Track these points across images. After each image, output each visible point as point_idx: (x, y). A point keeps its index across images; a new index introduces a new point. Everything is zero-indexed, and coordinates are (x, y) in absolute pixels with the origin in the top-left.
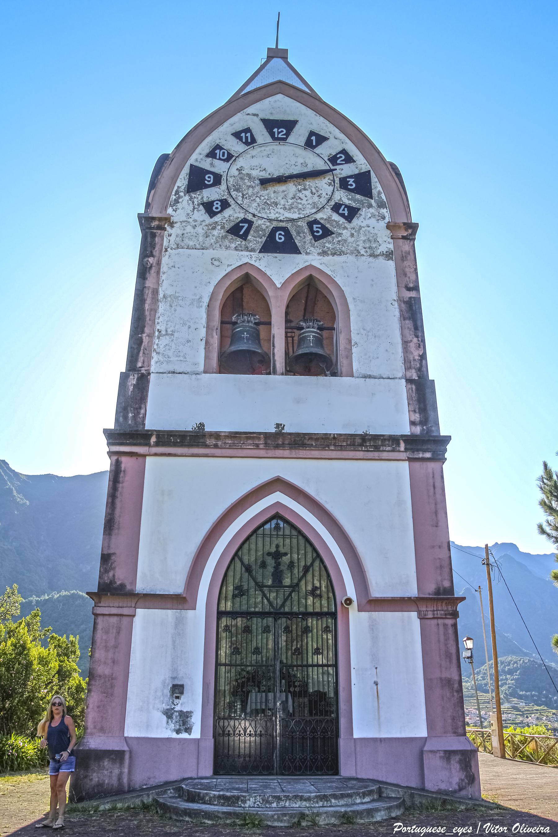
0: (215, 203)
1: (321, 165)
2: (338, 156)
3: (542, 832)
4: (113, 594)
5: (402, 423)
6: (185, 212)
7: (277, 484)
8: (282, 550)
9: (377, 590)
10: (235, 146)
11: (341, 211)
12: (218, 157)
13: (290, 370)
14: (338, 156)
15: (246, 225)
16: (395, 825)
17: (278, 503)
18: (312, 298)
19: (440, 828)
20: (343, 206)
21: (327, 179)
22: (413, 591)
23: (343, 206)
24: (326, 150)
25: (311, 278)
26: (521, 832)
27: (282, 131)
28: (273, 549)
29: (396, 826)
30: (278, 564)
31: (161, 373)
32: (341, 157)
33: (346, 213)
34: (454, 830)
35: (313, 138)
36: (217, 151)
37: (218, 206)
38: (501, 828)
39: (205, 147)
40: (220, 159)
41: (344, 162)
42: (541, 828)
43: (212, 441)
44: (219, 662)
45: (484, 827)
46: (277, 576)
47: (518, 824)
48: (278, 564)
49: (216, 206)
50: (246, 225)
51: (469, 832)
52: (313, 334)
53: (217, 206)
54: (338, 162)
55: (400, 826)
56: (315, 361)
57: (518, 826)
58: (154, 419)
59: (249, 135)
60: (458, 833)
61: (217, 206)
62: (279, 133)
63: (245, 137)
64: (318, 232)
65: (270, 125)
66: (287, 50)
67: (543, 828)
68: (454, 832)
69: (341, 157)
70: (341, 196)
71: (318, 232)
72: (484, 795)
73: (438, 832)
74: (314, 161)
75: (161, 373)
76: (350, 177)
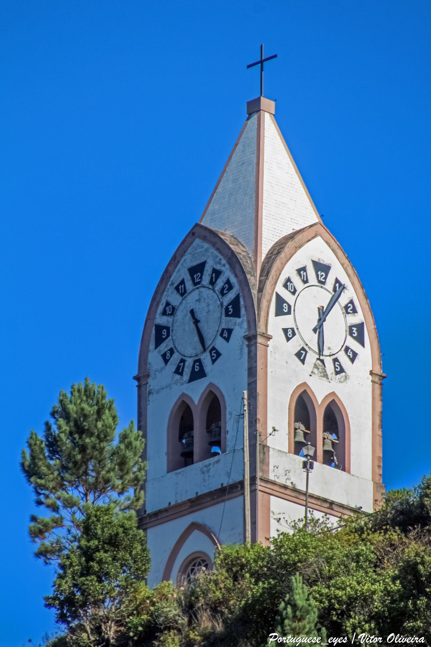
1: (208, 343)
3: (417, 642)
5: (305, 505)
10: (220, 283)
11: (224, 335)
15: (182, 364)
16: (271, 635)
18: (334, 419)
19: (315, 638)
20: (225, 330)
21: (199, 347)
24: (220, 344)
26: (396, 642)
27: (199, 275)
29: (271, 637)
31: (181, 354)
34: (329, 640)
35: (214, 275)
38: (376, 638)
39: (233, 280)
40: (169, 315)
42: (416, 638)
43: (63, 406)
45: (359, 637)
47: (392, 634)
51: (344, 642)
53: (290, 332)
55: (276, 637)
57: (392, 637)
60: (333, 643)
61: (290, 332)
62: (197, 277)
65: (360, 327)
67: (418, 638)
68: (330, 642)
69: (226, 287)
70: (189, 362)
71: (214, 356)
73: (314, 642)
74: (210, 330)
75: (181, 354)
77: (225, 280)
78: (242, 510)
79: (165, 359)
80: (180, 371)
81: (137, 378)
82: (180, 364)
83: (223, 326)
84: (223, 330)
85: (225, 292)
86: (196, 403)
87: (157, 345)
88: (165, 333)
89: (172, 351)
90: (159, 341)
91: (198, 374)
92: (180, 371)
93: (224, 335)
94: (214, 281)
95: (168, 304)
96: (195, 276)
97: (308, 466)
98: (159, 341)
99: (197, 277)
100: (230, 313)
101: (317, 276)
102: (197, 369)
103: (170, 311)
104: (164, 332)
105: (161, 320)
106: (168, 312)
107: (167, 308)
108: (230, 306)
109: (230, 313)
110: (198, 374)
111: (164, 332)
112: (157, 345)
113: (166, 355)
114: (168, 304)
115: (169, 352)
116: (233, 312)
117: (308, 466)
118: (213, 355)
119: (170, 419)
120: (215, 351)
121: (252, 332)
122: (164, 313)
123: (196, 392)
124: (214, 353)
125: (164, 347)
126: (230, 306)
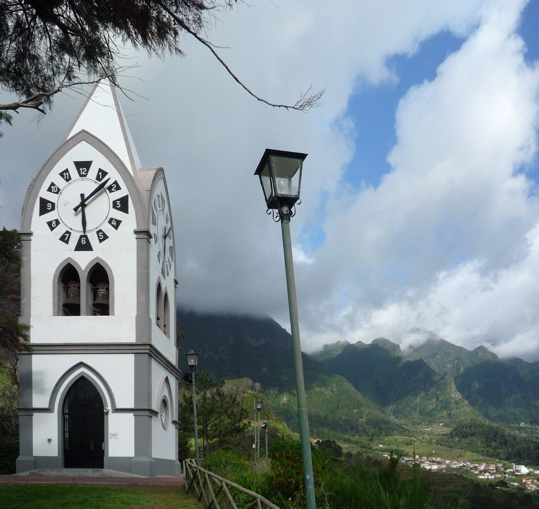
7: (81, 364)
11: (112, 223)
15: (68, 235)
17: (83, 372)
18: (100, 275)
22: (132, 406)
25: (69, 264)
33: (115, 224)
35: (100, 173)
36: (52, 187)
37: (54, 223)
40: (54, 192)
49: (53, 223)
53: (54, 223)
54: (113, 190)
56: (102, 308)
59: (67, 174)
61: (54, 223)
62: (83, 171)
63: (65, 175)
64: (101, 237)
66: (267, 149)
71: (101, 237)
72: (471, 349)
76: (118, 200)
79: (52, 225)
88: (50, 206)
90: (44, 210)
91: (84, 246)
93: (112, 223)
95: (53, 184)
98: (44, 210)
101: (79, 172)
102: (84, 242)
108: (119, 202)
114: (53, 184)
122: (50, 190)
123: (83, 261)
125: (50, 216)
126: (119, 202)
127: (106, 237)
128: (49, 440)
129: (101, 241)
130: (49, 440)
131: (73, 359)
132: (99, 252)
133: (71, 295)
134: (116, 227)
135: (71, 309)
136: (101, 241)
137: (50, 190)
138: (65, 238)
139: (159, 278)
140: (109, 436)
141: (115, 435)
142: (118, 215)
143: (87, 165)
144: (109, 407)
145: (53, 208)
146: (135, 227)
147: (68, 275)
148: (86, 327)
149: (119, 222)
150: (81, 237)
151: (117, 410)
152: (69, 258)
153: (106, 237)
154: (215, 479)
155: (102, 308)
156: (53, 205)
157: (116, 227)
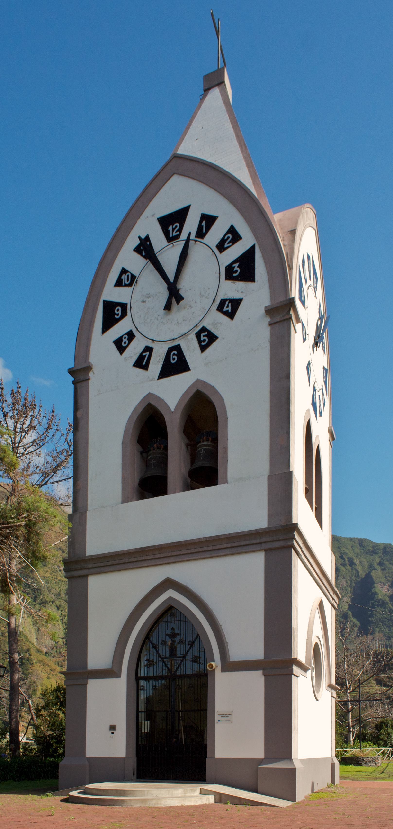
0: (123, 339)
2: (226, 238)
4: (141, 453)
6: (102, 344)
8: (176, 631)
9: (235, 654)
11: (225, 309)
12: (123, 284)
13: (189, 487)
14: (226, 238)
15: (147, 354)
18: (203, 415)
20: (227, 302)
23: (227, 302)
27: (176, 227)
28: (169, 632)
30: (173, 641)
32: (228, 238)
33: (229, 309)
35: (204, 223)
39: (243, 229)
40: (126, 285)
41: (231, 244)
44: (139, 676)
46: (173, 649)
48: (173, 641)
50: (147, 354)
52: (205, 447)
56: (205, 473)
58: (94, 546)
62: (173, 230)
69: (228, 238)
71: (204, 341)
76: (235, 262)
77: (236, 296)
78: (209, 245)
79: (120, 345)
80: (144, 363)
81: (71, 372)
82: (144, 354)
83: (207, 324)
84: (223, 302)
85: (226, 245)
86: (172, 408)
87: (106, 327)
88: (120, 312)
89: (131, 336)
90: (109, 322)
91: (175, 364)
92: (144, 363)
93: (225, 309)
94: (204, 231)
95: (124, 271)
96: (170, 228)
97: (362, 736)
98: (109, 322)
99: (173, 230)
100: (235, 275)
101: (166, 233)
102: (174, 359)
103: (128, 280)
104: (118, 310)
105: (111, 293)
106: (125, 281)
107: (123, 277)
108: (237, 265)
109: (235, 275)
110: (175, 364)
111: (118, 311)
112: (106, 327)
113: (122, 341)
114: (124, 271)
115: (124, 345)
116: (232, 237)
117: (362, 736)
118: (202, 339)
119: (124, 443)
120: (206, 333)
121: (281, 299)
122: (119, 283)
123: (172, 393)
124: (204, 336)
125: (119, 329)
126: (237, 265)
127: (212, 338)
128: (113, 728)
129: (203, 348)
130: (113, 728)
131: (151, 576)
132: (202, 368)
133: (153, 461)
134: (231, 315)
135: (151, 485)
136: (203, 348)
137: (119, 283)
138: (142, 363)
139: (308, 411)
140: (217, 718)
141: (226, 715)
142: (232, 289)
143: (180, 216)
144: (217, 663)
145: (124, 314)
146: (267, 302)
147: (149, 426)
148: (183, 513)
149: (236, 303)
150: (170, 350)
151: (229, 666)
152: (150, 395)
153: (212, 338)
154: (337, 602)
155: (205, 473)
156: (124, 306)
157: (231, 315)
